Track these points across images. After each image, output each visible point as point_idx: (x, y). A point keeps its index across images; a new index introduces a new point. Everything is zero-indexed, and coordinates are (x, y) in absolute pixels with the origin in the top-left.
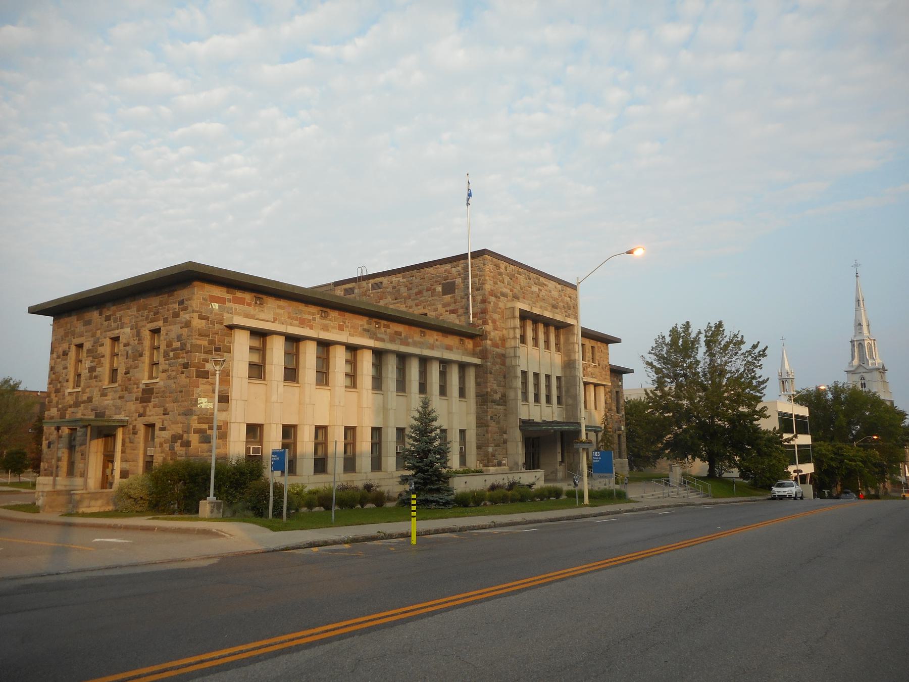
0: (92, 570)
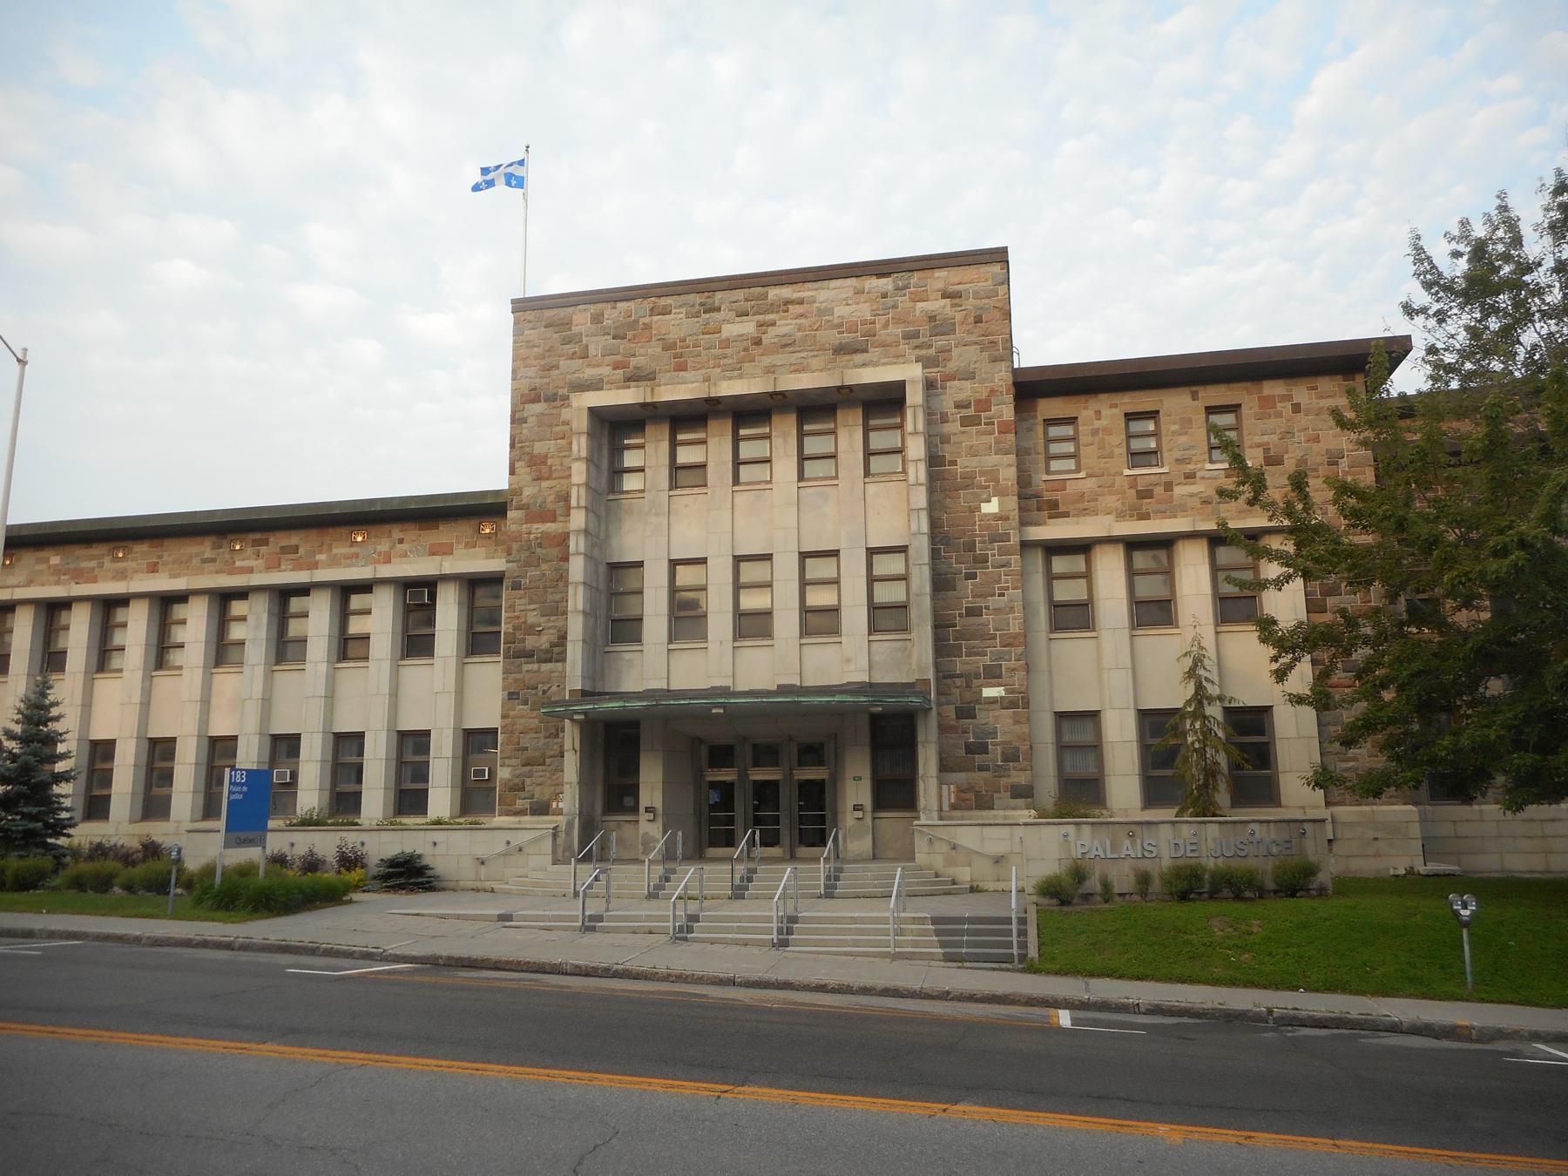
0: (505, 893)
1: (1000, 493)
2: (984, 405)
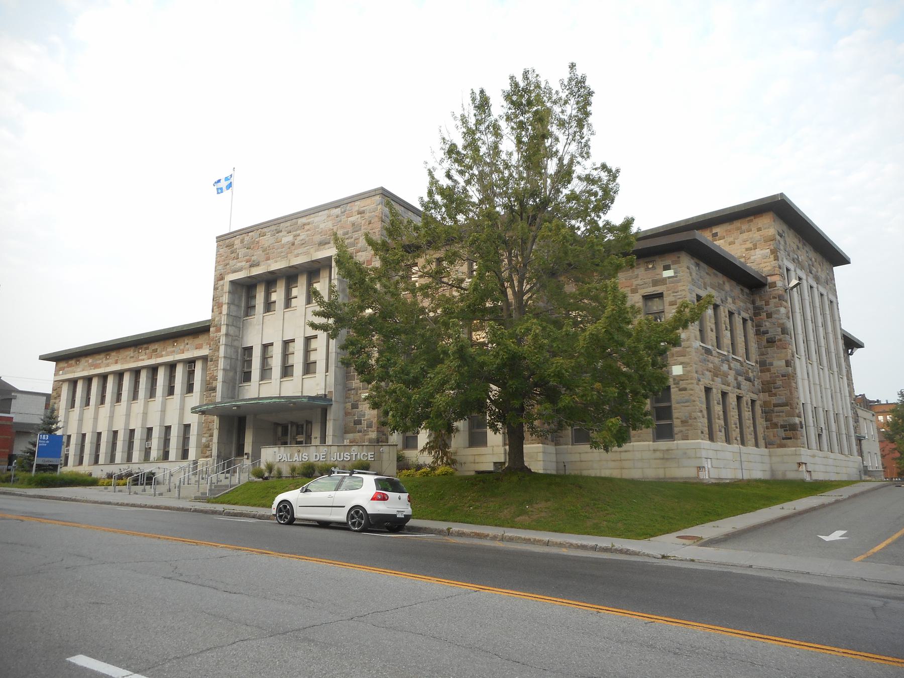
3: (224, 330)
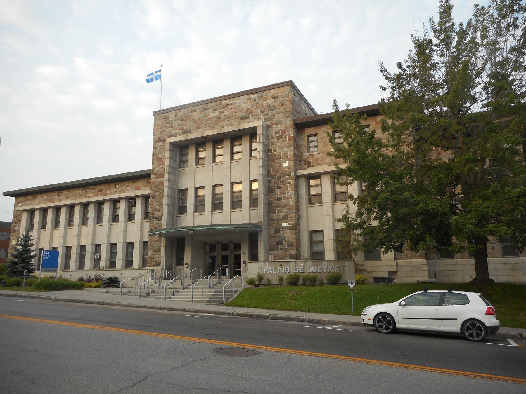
1: (288, 160)
2: (284, 132)
3: (166, 176)
